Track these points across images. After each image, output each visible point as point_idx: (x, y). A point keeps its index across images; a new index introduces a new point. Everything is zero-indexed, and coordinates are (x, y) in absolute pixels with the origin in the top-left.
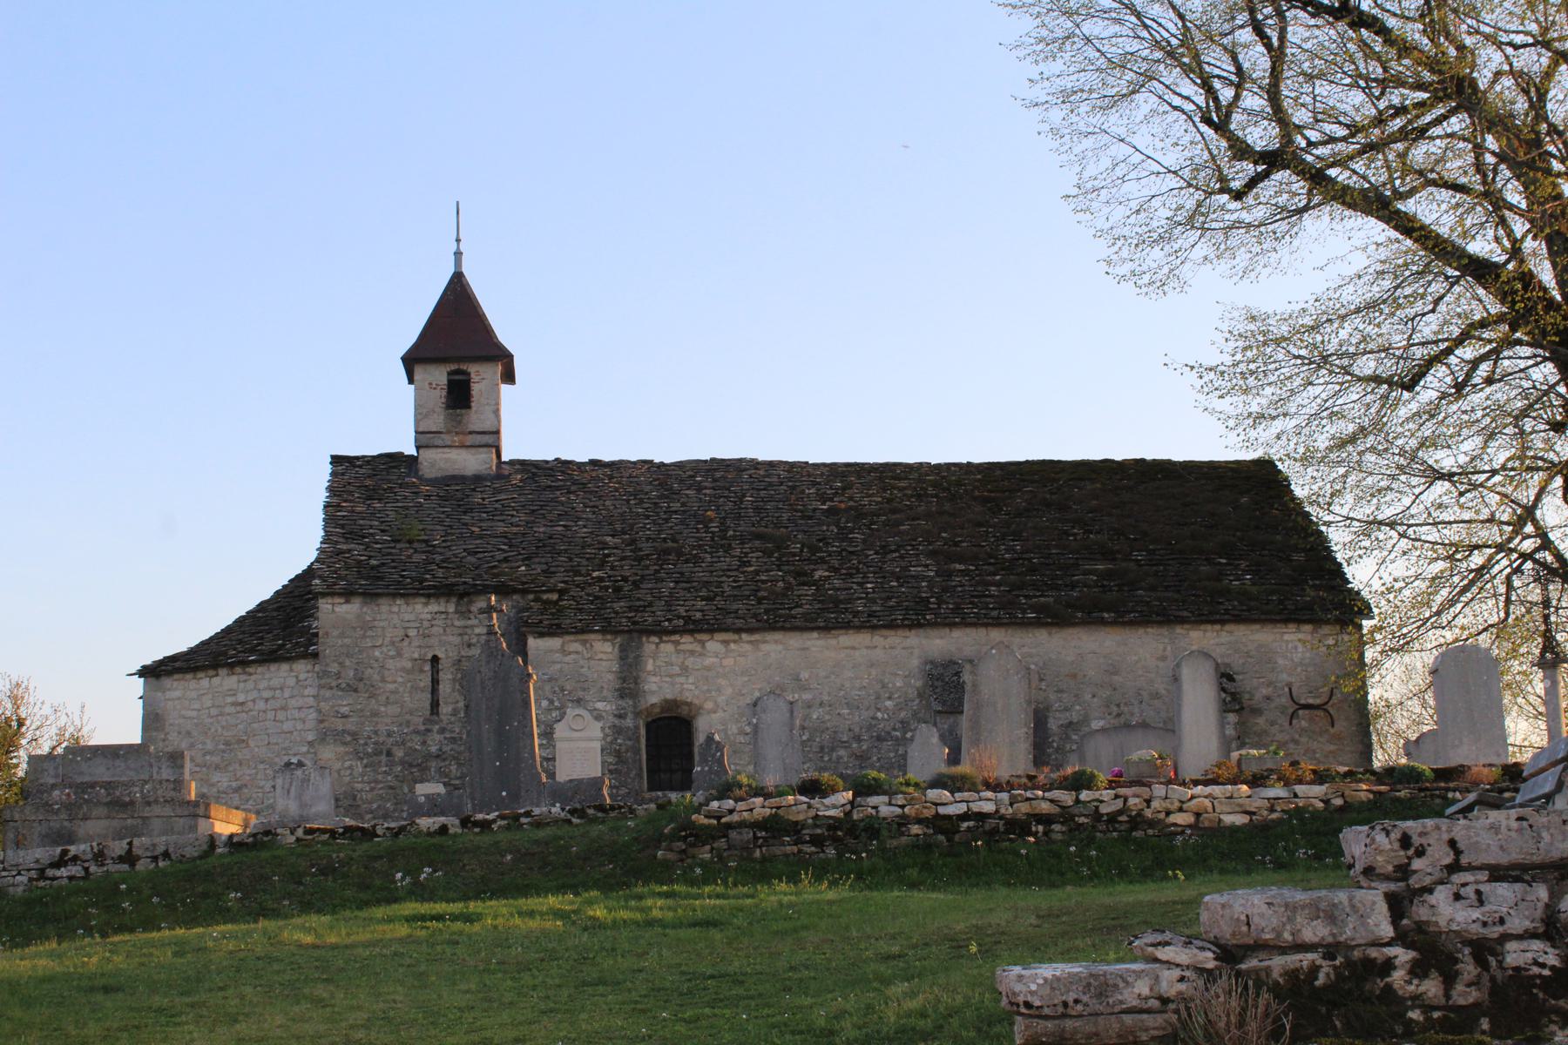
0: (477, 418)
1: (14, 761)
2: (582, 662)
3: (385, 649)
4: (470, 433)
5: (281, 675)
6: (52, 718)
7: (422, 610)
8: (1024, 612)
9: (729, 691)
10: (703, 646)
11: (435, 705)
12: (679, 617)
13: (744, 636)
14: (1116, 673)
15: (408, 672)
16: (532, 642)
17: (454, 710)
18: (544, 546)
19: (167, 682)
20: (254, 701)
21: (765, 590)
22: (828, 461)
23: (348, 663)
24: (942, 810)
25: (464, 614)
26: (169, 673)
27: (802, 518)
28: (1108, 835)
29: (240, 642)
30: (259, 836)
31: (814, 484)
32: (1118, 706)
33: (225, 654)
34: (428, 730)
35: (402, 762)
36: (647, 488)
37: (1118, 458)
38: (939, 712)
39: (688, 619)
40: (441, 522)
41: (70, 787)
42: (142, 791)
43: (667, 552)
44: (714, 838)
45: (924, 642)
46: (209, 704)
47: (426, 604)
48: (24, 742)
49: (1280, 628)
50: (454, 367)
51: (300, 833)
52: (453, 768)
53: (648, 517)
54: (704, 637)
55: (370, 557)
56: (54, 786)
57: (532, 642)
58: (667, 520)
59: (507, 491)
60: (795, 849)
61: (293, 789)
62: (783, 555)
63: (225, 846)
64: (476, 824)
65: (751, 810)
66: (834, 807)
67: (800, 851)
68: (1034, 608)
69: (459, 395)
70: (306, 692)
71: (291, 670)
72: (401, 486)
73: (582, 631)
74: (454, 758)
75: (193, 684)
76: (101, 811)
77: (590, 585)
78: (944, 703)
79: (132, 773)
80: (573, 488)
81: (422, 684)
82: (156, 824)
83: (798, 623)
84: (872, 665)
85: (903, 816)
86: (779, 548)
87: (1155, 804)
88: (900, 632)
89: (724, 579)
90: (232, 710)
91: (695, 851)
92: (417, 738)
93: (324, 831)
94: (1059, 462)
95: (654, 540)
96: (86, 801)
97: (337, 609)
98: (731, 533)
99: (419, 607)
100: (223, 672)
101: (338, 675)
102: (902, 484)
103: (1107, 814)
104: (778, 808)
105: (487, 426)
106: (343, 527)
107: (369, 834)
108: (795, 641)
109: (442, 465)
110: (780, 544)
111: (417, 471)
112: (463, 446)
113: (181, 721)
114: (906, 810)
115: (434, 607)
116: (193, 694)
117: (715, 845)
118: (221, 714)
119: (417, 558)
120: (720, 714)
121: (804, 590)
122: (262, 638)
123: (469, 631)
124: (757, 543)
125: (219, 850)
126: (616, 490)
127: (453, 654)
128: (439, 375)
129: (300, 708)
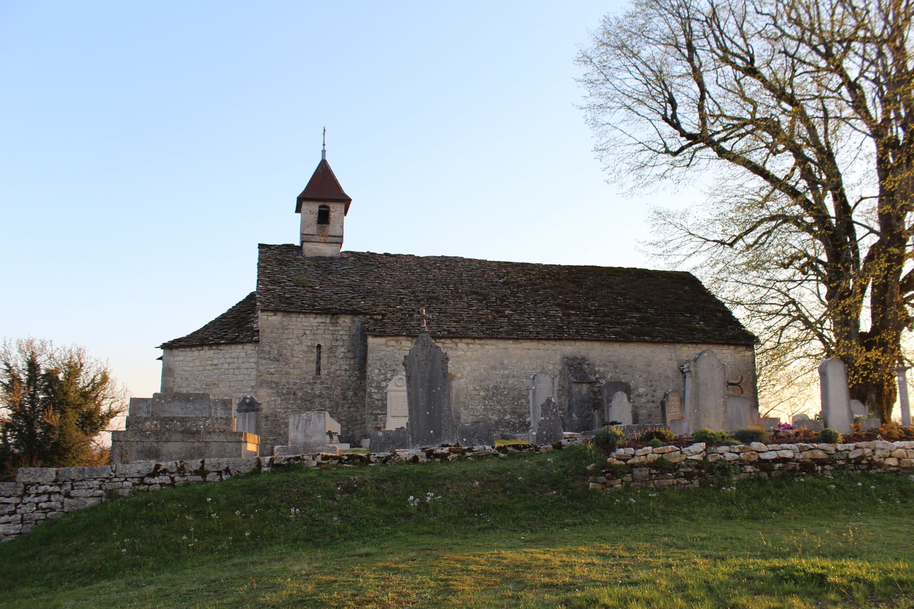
0: (332, 229)
2: (396, 351)
3: (294, 340)
4: (329, 236)
5: (236, 351)
6: (95, 363)
7: (313, 321)
8: (609, 335)
9: (469, 368)
10: (457, 346)
11: (318, 370)
12: (444, 330)
14: (650, 366)
15: (305, 352)
16: (371, 340)
17: (328, 372)
19: (176, 352)
20: (222, 364)
21: (484, 318)
22: (496, 260)
23: (274, 346)
24: (762, 456)
25: (335, 324)
26: (177, 348)
27: (493, 285)
28: (855, 472)
29: (215, 333)
30: (292, 460)
31: (493, 270)
33: (207, 339)
34: (315, 383)
35: (301, 399)
36: (415, 268)
37: (625, 267)
38: (574, 382)
39: (449, 331)
40: (317, 278)
41: (157, 420)
42: (205, 425)
43: (431, 298)
44: (624, 474)
47: (315, 318)
48: (82, 373)
49: (721, 347)
50: (322, 204)
51: (319, 458)
52: (327, 402)
53: (418, 281)
55: (285, 293)
56: (146, 419)
57: (371, 340)
58: (428, 283)
59: (347, 265)
60: (675, 481)
61: (300, 425)
62: (488, 302)
63: (268, 466)
64: (437, 456)
65: (646, 455)
66: (696, 453)
67: (678, 483)
68: (613, 333)
69: (324, 218)
70: (251, 360)
71: (243, 349)
72: (295, 259)
73: (397, 335)
75: (189, 354)
76: (178, 436)
77: (396, 312)
78: (576, 378)
79: (198, 412)
80: (380, 265)
81: (312, 359)
82: (214, 447)
83: (504, 335)
84: (538, 358)
85: (740, 460)
86: (485, 299)
87: (878, 453)
88: (552, 342)
90: (211, 368)
91: (611, 482)
92: (309, 387)
93: (335, 458)
95: (424, 292)
96: (168, 430)
97: (270, 318)
98: (460, 291)
99: (311, 319)
100: (206, 348)
101: (269, 353)
102: (533, 272)
103: (854, 459)
104: (662, 454)
105: (337, 233)
106: (269, 278)
107: (365, 461)
108: (501, 344)
109: (315, 251)
110: (486, 297)
111: (302, 253)
112: (325, 242)
113: (183, 372)
114: (741, 455)
115: (319, 320)
116: (190, 359)
117: (624, 479)
118: (204, 370)
119: (308, 295)
121: (502, 320)
122: (226, 332)
123: (336, 333)
124: (474, 296)
125: (265, 469)
126: (401, 267)
127: (328, 344)
128: (315, 207)
129: (247, 369)
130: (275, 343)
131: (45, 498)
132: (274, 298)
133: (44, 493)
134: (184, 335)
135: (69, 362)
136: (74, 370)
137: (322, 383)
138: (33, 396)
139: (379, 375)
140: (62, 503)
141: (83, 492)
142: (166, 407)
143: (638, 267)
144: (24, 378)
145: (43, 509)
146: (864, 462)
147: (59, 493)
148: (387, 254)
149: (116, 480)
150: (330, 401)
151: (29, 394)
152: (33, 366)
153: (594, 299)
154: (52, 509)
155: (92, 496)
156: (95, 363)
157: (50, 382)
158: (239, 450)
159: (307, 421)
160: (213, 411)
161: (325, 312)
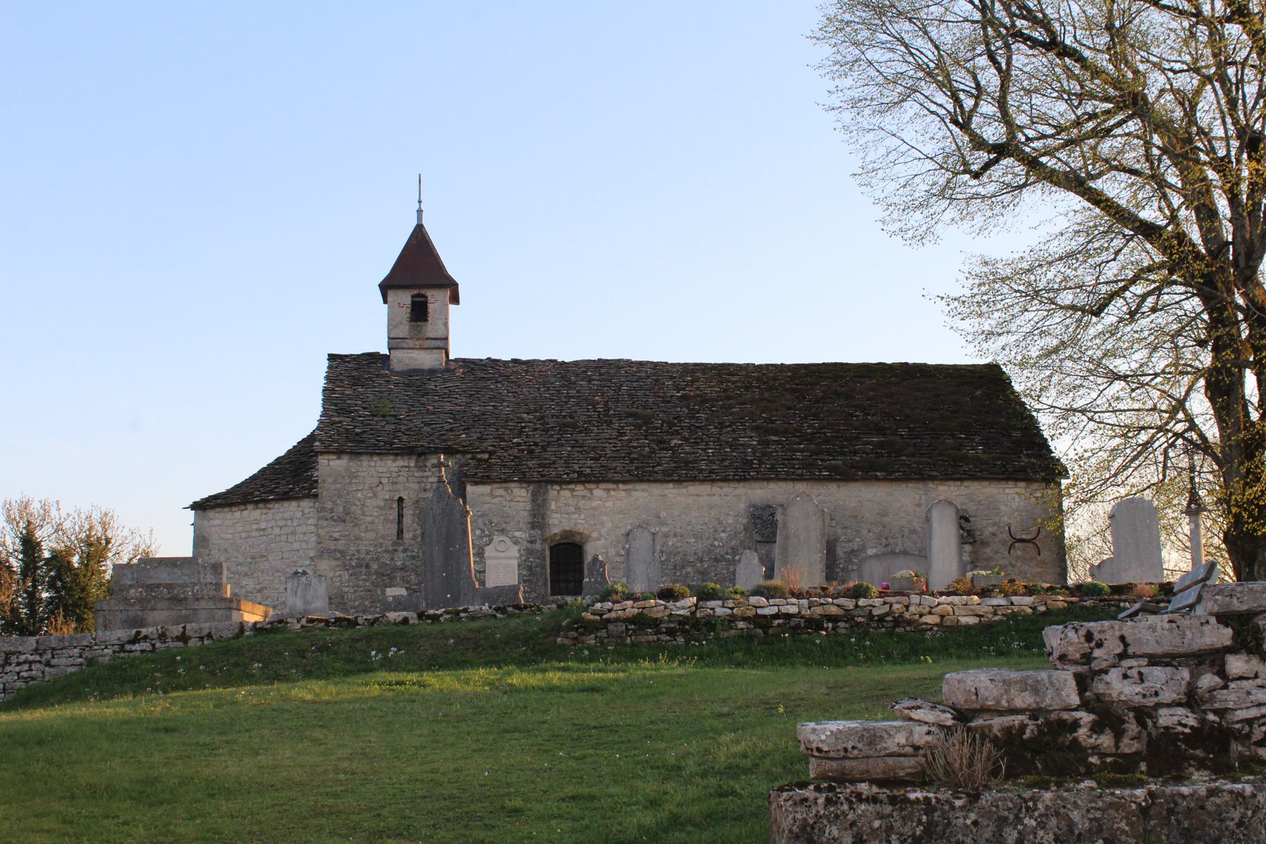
0: (431, 329)
1: (103, 568)
3: (365, 492)
4: (427, 339)
5: (291, 509)
6: (130, 538)
7: (391, 465)
8: (820, 471)
10: (592, 493)
11: (400, 532)
12: (575, 472)
13: (621, 486)
15: (381, 508)
16: (470, 489)
18: (479, 420)
19: (211, 513)
20: (272, 528)
22: (682, 362)
23: (338, 502)
24: (760, 611)
25: (422, 468)
26: (213, 507)
27: (663, 402)
28: (879, 630)
29: (263, 486)
31: (671, 378)
32: (887, 538)
33: (252, 494)
34: (396, 550)
35: (377, 573)
36: (553, 380)
38: (759, 542)
39: (580, 473)
41: (142, 587)
43: (566, 425)
44: (598, 629)
45: (749, 491)
46: (241, 529)
47: (394, 461)
48: (110, 555)
49: (1003, 484)
50: (416, 292)
51: (304, 621)
52: (413, 577)
53: (553, 400)
54: (593, 486)
55: (355, 427)
56: (131, 586)
57: (470, 489)
58: (566, 403)
59: (452, 380)
64: (429, 617)
65: (624, 610)
66: (684, 608)
67: (658, 639)
68: (827, 468)
69: (419, 312)
70: (309, 522)
71: (299, 506)
73: (506, 481)
74: (413, 570)
75: (229, 515)
76: (165, 604)
78: (763, 535)
79: (186, 578)
80: (500, 379)
81: (391, 517)
85: (732, 615)
86: (646, 423)
87: (912, 609)
88: (733, 485)
89: (607, 445)
91: (584, 638)
92: (387, 556)
93: (320, 621)
94: (847, 364)
95: (557, 417)
96: (154, 597)
97: (332, 463)
98: (612, 412)
99: (389, 463)
100: (250, 507)
101: (332, 511)
104: (644, 608)
105: (440, 334)
106: (336, 405)
108: (657, 489)
110: (647, 420)
111: (389, 366)
113: (221, 541)
115: (401, 462)
116: (230, 523)
120: (603, 541)
121: (663, 453)
122: (278, 483)
123: (425, 480)
124: (631, 420)
125: (247, 633)
127: (414, 497)
128: (405, 298)
129: (304, 533)
130: (340, 496)
131: (26, 667)
132: (339, 435)
133: (25, 662)
134: (223, 490)
135: (88, 536)
136: (96, 548)
137: (405, 551)
138: (32, 596)
139: (481, 537)
140: (43, 672)
141: (63, 661)
142: (152, 572)
143: (911, 361)
144: (15, 564)
145: (24, 678)
146: (889, 618)
147: (40, 662)
148: (515, 361)
149: (96, 647)
150: (417, 575)
151: (25, 591)
152: (29, 544)
153: (816, 417)
154: (33, 678)
155: (72, 665)
156: (130, 538)
157: (59, 571)
158: (229, 618)
159: (306, 585)
160: (202, 575)
161: (407, 451)
